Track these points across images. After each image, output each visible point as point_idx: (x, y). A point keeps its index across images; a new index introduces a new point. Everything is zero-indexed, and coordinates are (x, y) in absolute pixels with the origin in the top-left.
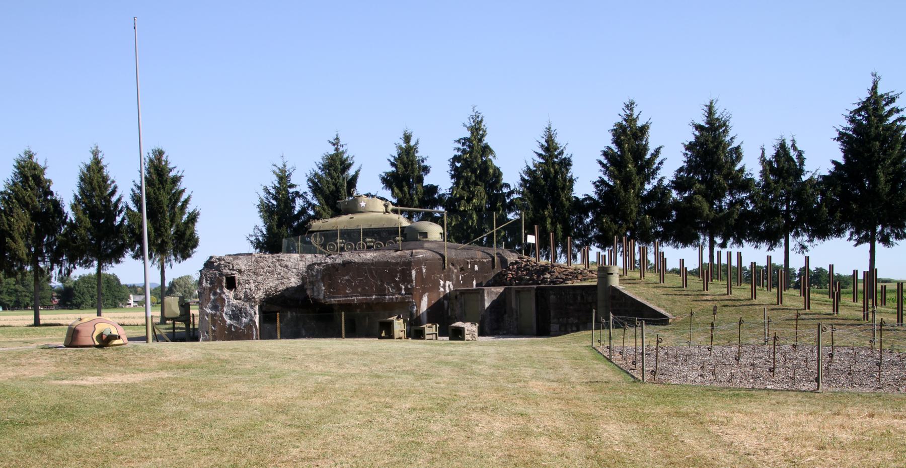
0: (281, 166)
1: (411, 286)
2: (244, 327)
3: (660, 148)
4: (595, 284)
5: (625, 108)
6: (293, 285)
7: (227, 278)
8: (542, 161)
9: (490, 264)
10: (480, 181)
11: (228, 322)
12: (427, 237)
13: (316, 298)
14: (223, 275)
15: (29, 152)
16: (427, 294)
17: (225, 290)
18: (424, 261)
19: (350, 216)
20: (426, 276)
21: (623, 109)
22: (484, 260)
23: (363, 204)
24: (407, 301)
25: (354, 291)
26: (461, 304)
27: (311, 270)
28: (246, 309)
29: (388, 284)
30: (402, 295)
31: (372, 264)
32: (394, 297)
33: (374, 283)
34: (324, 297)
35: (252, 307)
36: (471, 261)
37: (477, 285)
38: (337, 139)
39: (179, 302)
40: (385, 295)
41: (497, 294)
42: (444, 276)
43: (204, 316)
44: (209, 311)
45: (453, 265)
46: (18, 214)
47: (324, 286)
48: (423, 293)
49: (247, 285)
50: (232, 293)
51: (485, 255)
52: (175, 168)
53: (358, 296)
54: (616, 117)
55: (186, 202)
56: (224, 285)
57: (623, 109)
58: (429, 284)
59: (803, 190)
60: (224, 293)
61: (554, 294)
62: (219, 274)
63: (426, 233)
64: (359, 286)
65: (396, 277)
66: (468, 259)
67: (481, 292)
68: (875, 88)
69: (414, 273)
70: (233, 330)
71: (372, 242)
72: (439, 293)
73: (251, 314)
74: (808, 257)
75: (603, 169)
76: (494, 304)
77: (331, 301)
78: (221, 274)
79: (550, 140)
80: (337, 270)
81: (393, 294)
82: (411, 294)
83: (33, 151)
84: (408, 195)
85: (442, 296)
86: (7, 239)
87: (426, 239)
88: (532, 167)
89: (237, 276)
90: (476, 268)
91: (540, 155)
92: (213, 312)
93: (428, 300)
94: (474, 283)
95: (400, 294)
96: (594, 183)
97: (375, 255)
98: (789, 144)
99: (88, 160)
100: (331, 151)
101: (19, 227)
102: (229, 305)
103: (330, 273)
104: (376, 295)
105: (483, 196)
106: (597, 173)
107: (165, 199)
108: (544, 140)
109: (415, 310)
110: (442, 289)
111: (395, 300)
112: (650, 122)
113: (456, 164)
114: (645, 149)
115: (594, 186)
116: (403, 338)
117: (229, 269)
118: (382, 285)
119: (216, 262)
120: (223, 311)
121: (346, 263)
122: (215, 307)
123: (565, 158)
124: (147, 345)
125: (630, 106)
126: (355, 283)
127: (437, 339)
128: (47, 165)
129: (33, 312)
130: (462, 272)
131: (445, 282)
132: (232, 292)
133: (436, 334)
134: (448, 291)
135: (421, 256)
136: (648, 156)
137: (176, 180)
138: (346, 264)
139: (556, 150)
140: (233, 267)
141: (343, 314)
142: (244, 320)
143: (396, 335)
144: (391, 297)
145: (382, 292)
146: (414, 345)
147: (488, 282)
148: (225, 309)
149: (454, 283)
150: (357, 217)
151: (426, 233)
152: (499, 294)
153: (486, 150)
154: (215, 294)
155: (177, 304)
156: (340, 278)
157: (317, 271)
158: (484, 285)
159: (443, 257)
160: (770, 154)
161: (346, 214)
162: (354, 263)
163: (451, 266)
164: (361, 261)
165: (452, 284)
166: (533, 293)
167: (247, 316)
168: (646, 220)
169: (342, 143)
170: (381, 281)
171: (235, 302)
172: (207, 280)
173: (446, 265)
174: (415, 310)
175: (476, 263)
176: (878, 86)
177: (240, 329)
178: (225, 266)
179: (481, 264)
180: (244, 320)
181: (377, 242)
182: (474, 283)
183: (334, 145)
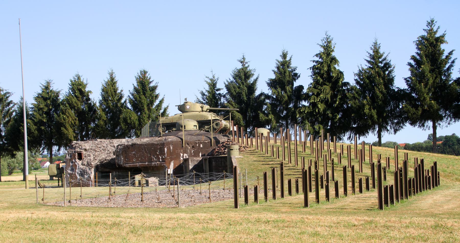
0: (211, 77)
1: (164, 156)
3: (452, 51)
10: (328, 82)
11: (78, 177)
13: (120, 164)
14: (76, 152)
15: (78, 75)
17: (77, 160)
18: (172, 143)
20: (173, 151)
22: (206, 141)
24: (162, 165)
28: (87, 170)
29: (154, 156)
30: (160, 162)
31: (146, 145)
32: (156, 163)
34: (123, 164)
35: (90, 169)
36: (198, 142)
38: (244, 58)
39: (56, 167)
40: (152, 162)
41: (197, 161)
42: (183, 151)
43: (67, 174)
44: (69, 172)
45: (188, 144)
46: (69, 113)
47: (123, 157)
48: (171, 161)
49: (89, 157)
50: (81, 162)
52: (153, 81)
54: (371, 44)
55: (161, 102)
56: (76, 157)
58: (174, 155)
60: (77, 162)
64: (139, 157)
66: (196, 141)
69: (166, 149)
72: (180, 161)
73: (89, 173)
79: (376, 51)
80: (129, 149)
81: (156, 162)
83: (80, 75)
85: (182, 162)
86: (62, 128)
89: (84, 152)
90: (201, 146)
91: (369, 62)
92: (71, 172)
93: (174, 165)
94: (200, 154)
95: (159, 161)
96: (405, 79)
97: (148, 139)
99: (107, 78)
100: (240, 66)
101: (69, 120)
102: (79, 169)
103: (125, 150)
104: (148, 162)
107: (145, 101)
114: (441, 53)
115: (405, 81)
118: (150, 156)
119: (74, 145)
120: (76, 172)
121: (133, 145)
122: (72, 170)
125: (431, 23)
128: (88, 82)
129: (22, 174)
130: (193, 148)
131: (184, 155)
132: (81, 161)
135: (170, 140)
136: (444, 57)
137: (154, 88)
138: (133, 145)
139: (380, 58)
141: (129, 173)
144: (155, 163)
145: (150, 161)
146: (360, 195)
148: (77, 171)
149: (189, 154)
152: (199, 161)
153: (334, 60)
154: (72, 162)
155: (55, 168)
159: (182, 139)
162: (137, 144)
163: (187, 145)
164: (141, 143)
165: (188, 155)
167: (87, 174)
168: (432, 104)
169: (246, 61)
170: (150, 154)
171: (82, 167)
172: (69, 155)
173: (184, 145)
175: (201, 143)
179: (204, 144)
180: (86, 176)
182: (200, 154)
183: (242, 62)
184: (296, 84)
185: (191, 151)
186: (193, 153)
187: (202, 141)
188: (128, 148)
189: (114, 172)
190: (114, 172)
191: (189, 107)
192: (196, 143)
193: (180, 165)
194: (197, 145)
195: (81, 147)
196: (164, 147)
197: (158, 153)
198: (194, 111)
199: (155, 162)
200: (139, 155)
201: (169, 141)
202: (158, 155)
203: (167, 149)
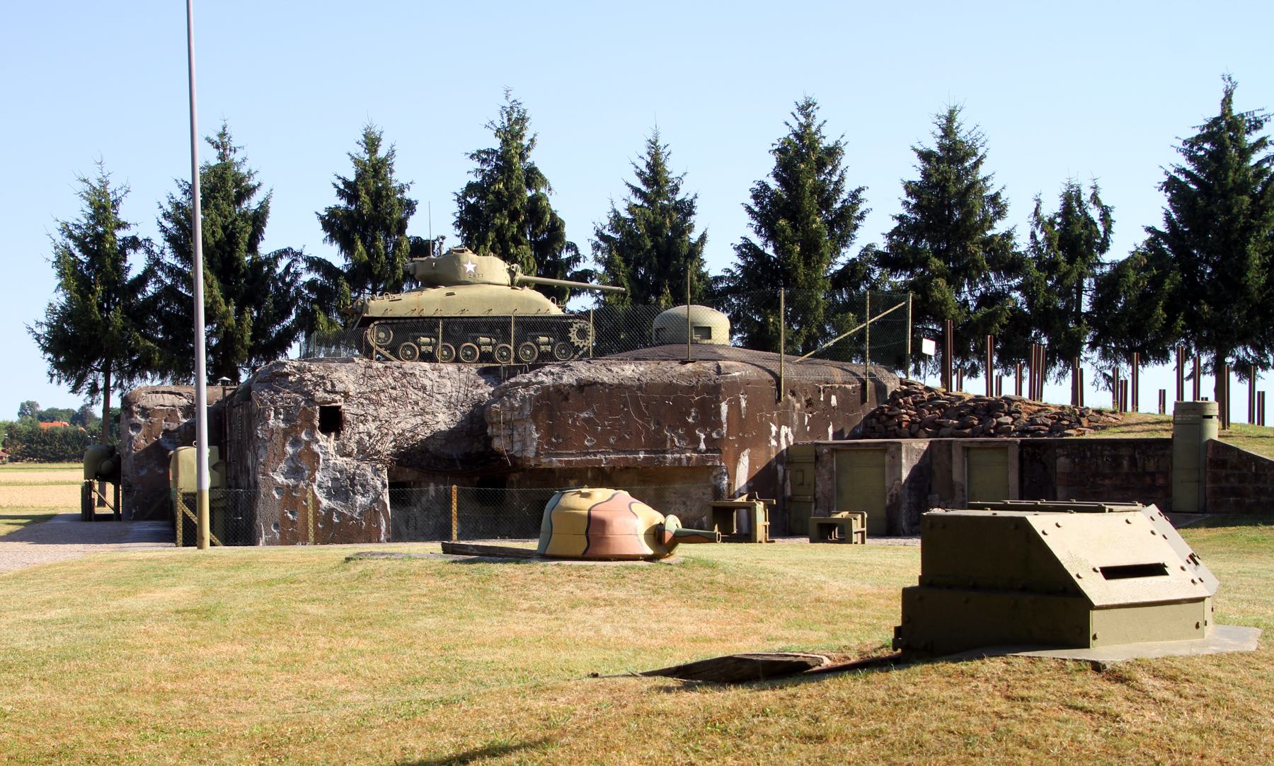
1: (718, 434)
2: (360, 514)
4: (1168, 436)
5: (796, 112)
6: (443, 427)
7: (323, 410)
8: (639, 202)
9: (858, 393)
11: (325, 503)
12: (710, 337)
13: (518, 455)
16: (747, 452)
17: (319, 435)
19: (443, 290)
21: (793, 114)
22: (847, 386)
23: (470, 267)
24: (710, 464)
25: (602, 440)
26: (831, 472)
27: (509, 397)
29: (673, 429)
30: (699, 452)
31: (640, 388)
32: (683, 456)
33: (643, 426)
34: (537, 454)
35: (376, 472)
36: (825, 388)
37: (836, 436)
40: (665, 452)
42: (779, 415)
44: (280, 479)
45: (794, 394)
47: (537, 430)
48: (742, 449)
51: (849, 377)
53: (609, 453)
54: (780, 129)
56: (317, 423)
57: (793, 114)
59: (1120, 276)
60: (317, 442)
61: (1067, 456)
62: (307, 402)
63: (709, 329)
64: (611, 433)
65: (689, 414)
66: (820, 382)
67: (892, 448)
68: (1227, 101)
69: (724, 408)
70: (336, 520)
71: (490, 344)
72: (769, 450)
73: (375, 488)
74: (1263, 393)
75: (755, 223)
76: (916, 471)
77: (551, 461)
78: (310, 399)
80: (566, 399)
81: (682, 451)
82: (719, 451)
84: (383, 257)
85: (773, 456)
87: (709, 341)
88: (625, 214)
91: (636, 191)
92: (291, 482)
93: (750, 464)
94: (830, 430)
95: (695, 450)
97: (642, 369)
98: (1086, 197)
100: (208, 156)
104: (646, 452)
105: (532, 266)
106: (744, 228)
108: (645, 163)
109: (725, 482)
110: (774, 443)
111: (684, 463)
112: (843, 141)
113: (468, 199)
116: (764, 541)
117: (325, 391)
118: (659, 431)
120: (314, 481)
121: (585, 385)
122: (295, 472)
123: (682, 201)
124: (200, 552)
125: (806, 109)
126: (603, 426)
127: (863, 542)
130: (810, 409)
131: (779, 428)
133: (862, 533)
134: (784, 446)
135: (737, 374)
138: (584, 387)
140: (333, 386)
142: (360, 500)
143: (758, 539)
144: (677, 455)
145: (657, 445)
147: (854, 428)
148: (318, 476)
149: (795, 429)
150: (460, 291)
151: (709, 329)
152: (922, 453)
153: (533, 177)
156: (572, 416)
157: (523, 399)
158: (846, 436)
159: (778, 379)
160: (1051, 207)
161: (434, 285)
163: (790, 397)
164: (616, 382)
165: (792, 432)
166: (1014, 453)
170: (658, 423)
172: (277, 413)
174: (725, 482)
175: (833, 391)
176: (1233, 98)
177: (352, 518)
178: (316, 384)
179: (843, 394)
180: (360, 500)
181: (501, 345)
182: (830, 430)
183: (218, 147)
184: (1000, 227)
185: (802, 418)
186: (808, 425)
187: (837, 386)
188: (561, 398)
189: (432, 484)
190: (432, 484)
191: (475, 268)
192: (820, 392)
193: (769, 465)
194: (822, 399)
195: (329, 385)
196: (717, 398)
197: (690, 420)
198: (492, 281)
199: (678, 452)
200: (609, 425)
201: (735, 377)
202: (690, 430)
203: (730, 407)
